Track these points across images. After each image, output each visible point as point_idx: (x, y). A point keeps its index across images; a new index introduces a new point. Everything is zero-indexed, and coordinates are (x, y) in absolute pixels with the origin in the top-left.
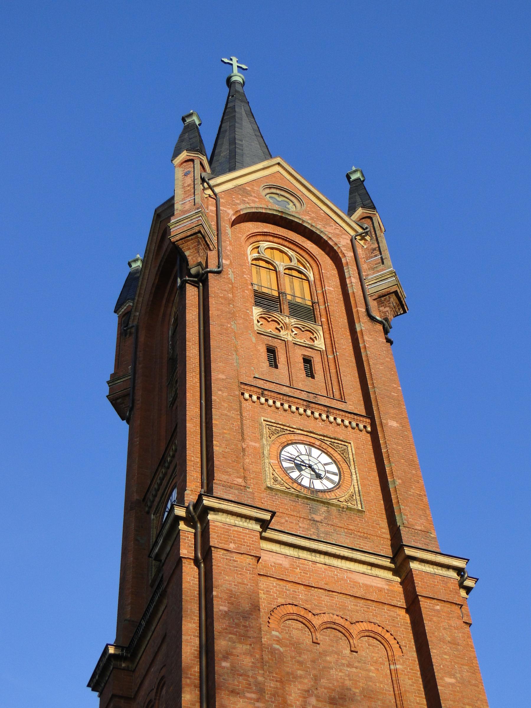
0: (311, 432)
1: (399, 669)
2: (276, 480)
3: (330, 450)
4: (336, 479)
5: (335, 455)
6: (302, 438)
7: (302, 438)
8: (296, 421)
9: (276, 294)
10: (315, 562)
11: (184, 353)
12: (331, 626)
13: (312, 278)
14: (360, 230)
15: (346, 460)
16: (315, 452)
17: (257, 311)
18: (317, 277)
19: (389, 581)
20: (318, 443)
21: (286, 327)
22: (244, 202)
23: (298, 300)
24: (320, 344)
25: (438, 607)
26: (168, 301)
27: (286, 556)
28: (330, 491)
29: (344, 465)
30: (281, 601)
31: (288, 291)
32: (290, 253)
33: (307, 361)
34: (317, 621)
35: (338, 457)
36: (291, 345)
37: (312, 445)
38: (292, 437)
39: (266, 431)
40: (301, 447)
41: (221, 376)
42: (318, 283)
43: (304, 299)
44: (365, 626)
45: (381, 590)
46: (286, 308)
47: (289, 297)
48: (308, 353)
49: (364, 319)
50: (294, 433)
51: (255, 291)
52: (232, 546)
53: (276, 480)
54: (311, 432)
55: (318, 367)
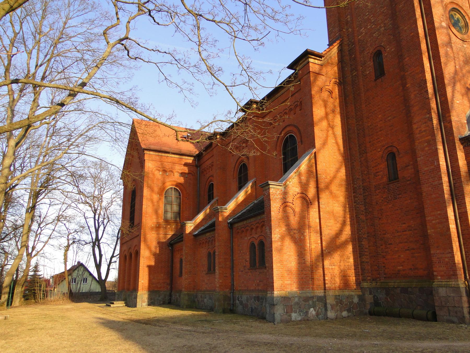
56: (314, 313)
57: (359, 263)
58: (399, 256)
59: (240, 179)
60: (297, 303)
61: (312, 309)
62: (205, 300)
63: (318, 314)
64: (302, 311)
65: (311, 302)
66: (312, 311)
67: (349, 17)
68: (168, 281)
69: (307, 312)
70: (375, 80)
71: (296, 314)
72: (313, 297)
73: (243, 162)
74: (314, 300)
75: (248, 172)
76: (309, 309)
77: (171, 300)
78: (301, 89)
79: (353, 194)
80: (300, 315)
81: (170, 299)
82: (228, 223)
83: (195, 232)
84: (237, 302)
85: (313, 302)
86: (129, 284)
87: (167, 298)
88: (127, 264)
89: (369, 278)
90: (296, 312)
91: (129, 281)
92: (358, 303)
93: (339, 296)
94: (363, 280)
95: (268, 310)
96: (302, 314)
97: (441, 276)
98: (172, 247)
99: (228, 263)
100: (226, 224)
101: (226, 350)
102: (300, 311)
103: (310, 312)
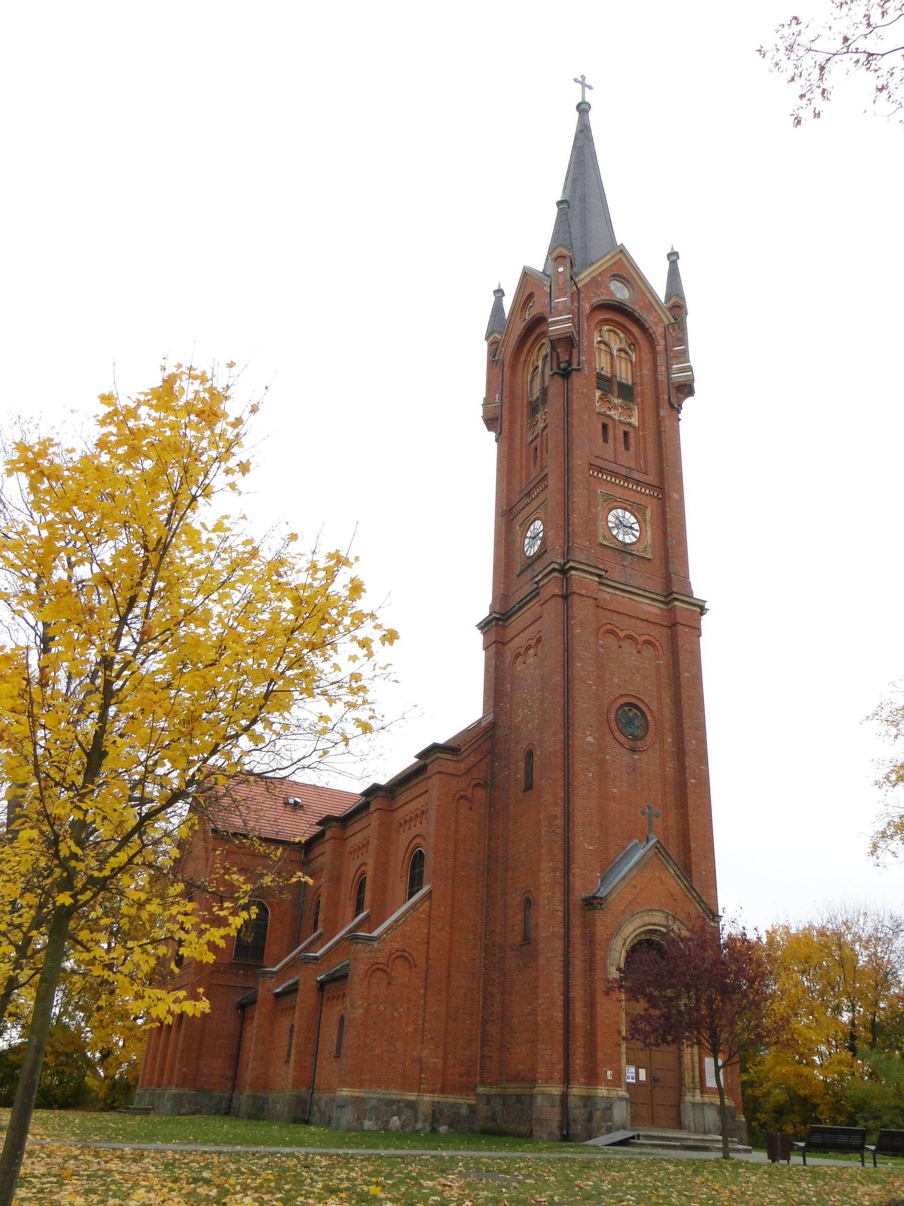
0: (626, 500)
1: (811, 1096)
2: (604, 537)
3: (636, 513)
4: (637, 534)
5: (639, 517)
6: (621, 504)
7: (621, 504)
8: (618, 492)
9: (609, 375)
10: (623, 597)
11: (710, 865)
12: (629, 637)
13: (634, 360)
14: (673, 321)
15: (645, 521)
16: (628, 514)
17: (598, 393)
18: (638, 359)
19: (661, 609)
20: (629, 508)
21: (615, 407)
22: (596, 295)
23: (624, 381)
24: (635, 421)
25: (686, 630)
26: (529, 351)
27: (609, 593)
28: (634, 543)
29: (643, 524)
30: (604, 621)
31: (618, 374)
32: (622, 335)
33: (626, 434)
34: (622, 634)
35: (640, 518)
36: (617, 423)
37: (626, 509)
38: (616, 504)
39: (601, 500)
40: (619, 510)
41: (579, 463)
42: (638, 364)
43: (627, 380)
44: (646, 637)
45: (656, 615)
46: (615, 388)
47: (618, 379)
48: (627, 429)
49: (667, 406)
50: (617, 501)
51: (598, 374)
52: (584, 592)
53: (604, 537)
54: (626, 500)
55: (632, 440)
56: (398, 1123)
57: (479, 1057)
58: (521, 1050)
59: (412, 878)
60: (375, 1108)
61: (396, 1118)
62: (278, 1107)
63: (403, 1126)
64: (379, 1119)
65: (395, 1107)
66: (395, 1121)
67: (508, 685)
68: (230, 1073)
69: (387, 1122)
70: (524, 791)
71: (370, 1123)
72: (399, 1101)
73: (418, 847)
74: (401, 1105)
75: (425, 868)
76: (392, 1116)
77: (230, 1108)
78: (427, 791)
79: (483, 954)
80: (377, 1124)
81: (229, 1107)
82: (318, 982)
83: (277, 988)
84: (315, 1108)
85: (399, 1108)
86: (162, 1075)
87: (224, 1105)
88: (162, 1037)
89: (490, 1081)
90: (370, 1120)
91: (162, 1070)
92: (467, 1116)
93: (439, 1102)
94: (480, 1083)
95: (334, 1115)
96: (379, 1123)
97: (542, 1079)
98: (243, 1012)
99: (310, 1045)
100: (314, 983)
101: (5, 909)
102: (377, 1119)
103: (391, 1122)
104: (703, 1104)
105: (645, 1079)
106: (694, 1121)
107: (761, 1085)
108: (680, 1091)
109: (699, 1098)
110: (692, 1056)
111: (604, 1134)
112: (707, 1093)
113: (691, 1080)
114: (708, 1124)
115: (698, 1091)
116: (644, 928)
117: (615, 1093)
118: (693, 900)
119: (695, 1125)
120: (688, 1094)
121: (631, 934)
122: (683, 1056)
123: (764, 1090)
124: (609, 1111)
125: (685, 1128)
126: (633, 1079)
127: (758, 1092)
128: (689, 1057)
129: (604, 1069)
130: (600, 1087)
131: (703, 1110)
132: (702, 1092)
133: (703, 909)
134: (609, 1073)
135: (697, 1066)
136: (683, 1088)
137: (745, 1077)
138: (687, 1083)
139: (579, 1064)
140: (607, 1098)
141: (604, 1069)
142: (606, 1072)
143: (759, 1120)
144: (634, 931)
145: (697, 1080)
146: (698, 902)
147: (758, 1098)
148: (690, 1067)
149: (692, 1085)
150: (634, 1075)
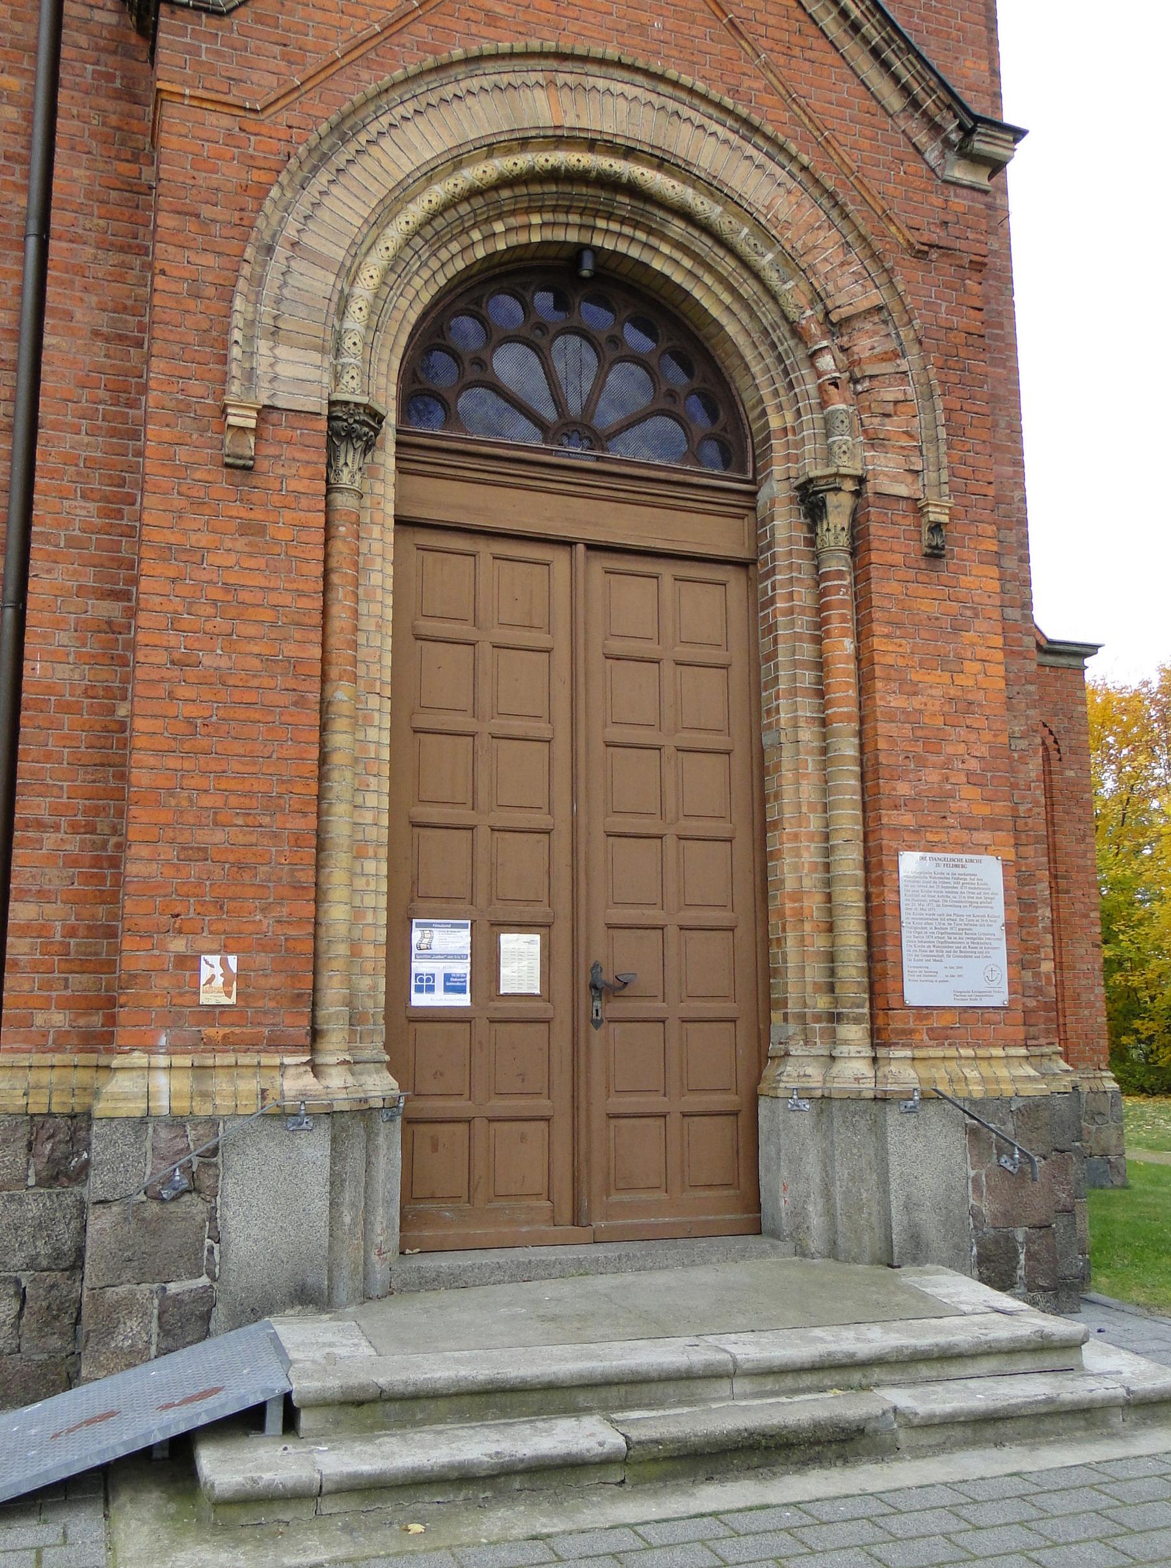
104: (882, 1099)
105: (534, 986)
106: (827, 1195)
107: (1143, 963)
108: (762, 1037)
109: (862, 1068)
110: (828, 852)
111: (134, 1357)
112: (906, 1037)
113: (815, 973)
114: (909, 1206)
115: (854, 1033)
116: (523, 161)
117: (249, 1085)
118: (849, 46)
119: (829, 1212)
120: (796, 1049)
121: (430, 175)
122: (777, 855)
123: (1149, 976)
124: (195, 1206)
125: (775, 1234)
126: (452, 986)
127: (1136, 981)
128: (810, 854)
129: (178, 945)
130: (139, 1058)
131: (878, 1129)
132: (878, 1037)
133: (905, 90)
134: (211, 968)
135: (851, 897)
136: (776, 1016)
137: (1108, 952)
138: (793, 994)
139: (41, 930)
140: (177, 1122)
141: (178, 945)
142: (189, 963)
143: (1137, 1031)
144: (456, 161)
145: (852, 970)
146: (875, 52)
147: (1135, 990)
148: (813, 904)
149: (822, 1003)
150: (463, 968)
